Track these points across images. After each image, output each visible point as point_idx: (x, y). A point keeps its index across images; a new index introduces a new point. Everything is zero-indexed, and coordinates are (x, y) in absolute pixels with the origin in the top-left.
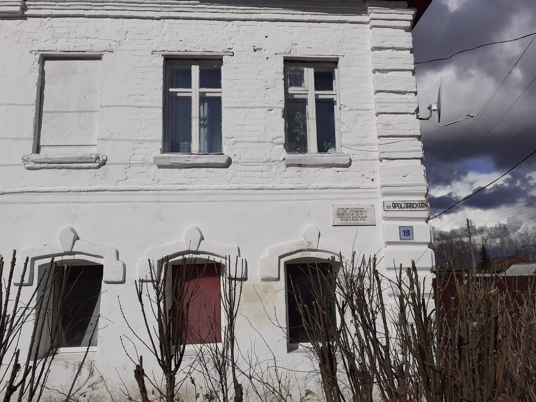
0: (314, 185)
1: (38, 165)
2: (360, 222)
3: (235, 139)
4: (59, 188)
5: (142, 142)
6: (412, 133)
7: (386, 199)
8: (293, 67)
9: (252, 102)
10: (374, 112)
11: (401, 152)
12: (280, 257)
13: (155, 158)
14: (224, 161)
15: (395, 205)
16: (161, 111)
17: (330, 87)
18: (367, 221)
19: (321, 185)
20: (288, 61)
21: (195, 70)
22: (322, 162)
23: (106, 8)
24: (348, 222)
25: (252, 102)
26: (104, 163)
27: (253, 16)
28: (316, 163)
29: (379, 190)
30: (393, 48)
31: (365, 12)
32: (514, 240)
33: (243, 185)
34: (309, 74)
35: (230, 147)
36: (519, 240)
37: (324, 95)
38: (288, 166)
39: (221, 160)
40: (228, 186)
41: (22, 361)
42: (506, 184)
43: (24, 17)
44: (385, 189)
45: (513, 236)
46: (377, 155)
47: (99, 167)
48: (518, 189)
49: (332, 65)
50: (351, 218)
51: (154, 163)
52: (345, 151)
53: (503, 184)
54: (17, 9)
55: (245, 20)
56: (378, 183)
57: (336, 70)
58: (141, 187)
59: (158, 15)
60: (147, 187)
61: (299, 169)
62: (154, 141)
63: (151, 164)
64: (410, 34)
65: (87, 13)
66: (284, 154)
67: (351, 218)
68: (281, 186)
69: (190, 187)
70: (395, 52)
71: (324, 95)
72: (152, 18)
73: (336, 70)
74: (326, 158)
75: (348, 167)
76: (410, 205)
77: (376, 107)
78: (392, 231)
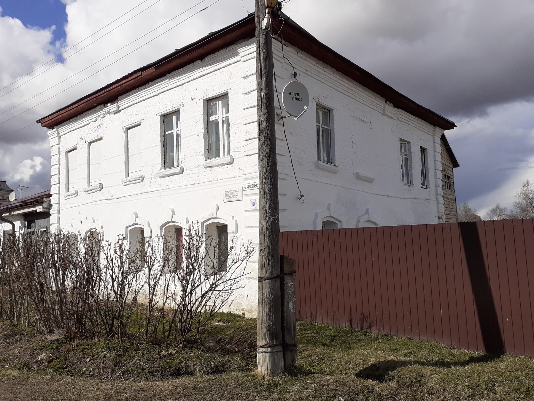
2: (235, 199)
12: (127, 227)
24: (232, 199)
31: (237, 54)
38: (205, 168)
39: (177, 170)
41: (365, 322)
43: (120, 111)
47: (142, 181)
54: (116, 109)
57: (38, 211)
65: (135, 102)
68: (203, 181)
69: (170, 187)
72: (155, 96)
75: (232, 164)
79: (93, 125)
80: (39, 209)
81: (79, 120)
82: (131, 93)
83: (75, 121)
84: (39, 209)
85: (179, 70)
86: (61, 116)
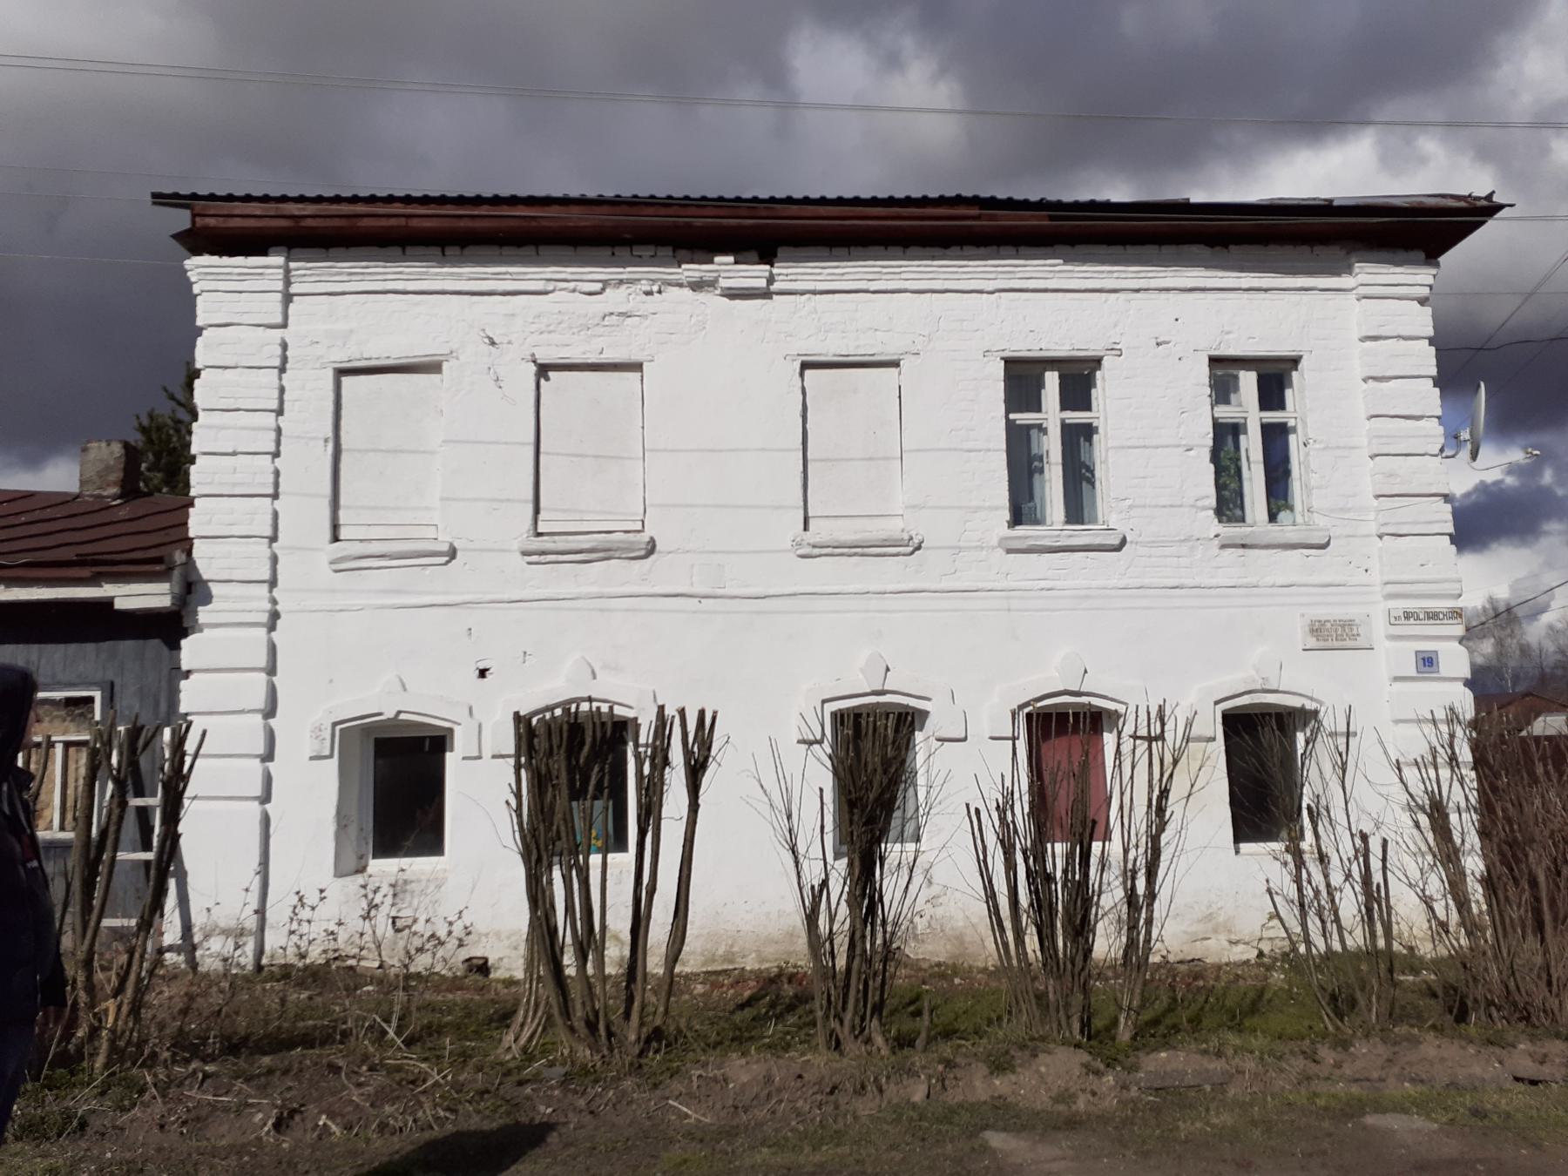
0: (1269, 580)
1: (817, 551)
2: (1349, 643)
3: (1128, 503)
4: (851, 588)
5: (977, 509)
6: (1434, 491)
7: (1392, 604)
8: (1223, 370)
9: (1152, 431)
10: (1366, 453)
11: (1416, 523)
12: (1216, 703)
13: (1003, 539)
14: (1117, 542)
15: (1408, 615)
16: (1004, 456)
17: (1281, 406)
18: (1360, 642)
19: (1281, 581)
20: (1215, 361)
21: (1052, 379)
22: (1282, 541)
23: (904, 276)
24: (1329, 644)
25: (1152, 431)
26: (919, 548)
27: (1154, 283)
28: (1276, 542)
29: (1378, 589)
30: (1399, 337)
31: (1348, 270)
32: (1534, 645)
33: (1147, 581)
34: (1248, 381)
35: (1123, 516)
36: (1550, 647)
37: (1273, 416)
38: (1223, 547)
40: (1122, 583)
42: (1510, 481)
44: (1390, 589)
45: (1534, 633)
46: (1373, 528)
48: (1546, 493)
49: (1288, 366)
50: (1332, 635)
51: (1000, 545)
52: (1320, 521)
53: (1501, 482)
55: (1138, 291)
56: (1376, 577)
57: (1294, 373)
58: (980, 585)
59: (991, 285)
60: (989, 586)
61: (1241, 551)
62: (997, 508)
63: (994, 548)
64: (1428, 310)
65: (874, 286)
66: (1215, 527)
67: (1332, 635)
68: (1214, 582)
69: (1058, 584)
70: (1402, 342)
71: (1273, 416)
72: (981, 292)
73: (1294, 373)
74: (1275, 532)
76: (1433, 616)
77: (1370, 443)
78: (1404, 657)
79: (562, 301)
80: (133, 596)
81: (1084, 260)
82: (507, 251)
83: (443, 261)
84: (133, 596)
85: (1118, 249)
86: (402, 221)
